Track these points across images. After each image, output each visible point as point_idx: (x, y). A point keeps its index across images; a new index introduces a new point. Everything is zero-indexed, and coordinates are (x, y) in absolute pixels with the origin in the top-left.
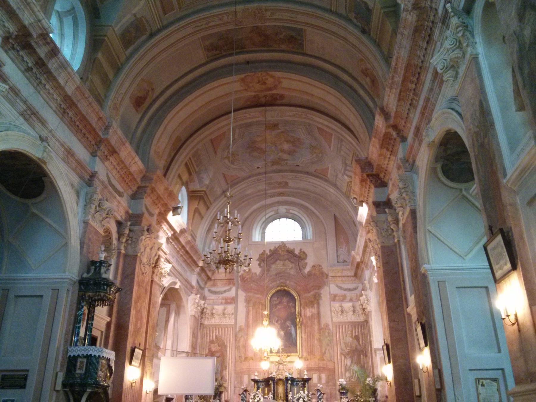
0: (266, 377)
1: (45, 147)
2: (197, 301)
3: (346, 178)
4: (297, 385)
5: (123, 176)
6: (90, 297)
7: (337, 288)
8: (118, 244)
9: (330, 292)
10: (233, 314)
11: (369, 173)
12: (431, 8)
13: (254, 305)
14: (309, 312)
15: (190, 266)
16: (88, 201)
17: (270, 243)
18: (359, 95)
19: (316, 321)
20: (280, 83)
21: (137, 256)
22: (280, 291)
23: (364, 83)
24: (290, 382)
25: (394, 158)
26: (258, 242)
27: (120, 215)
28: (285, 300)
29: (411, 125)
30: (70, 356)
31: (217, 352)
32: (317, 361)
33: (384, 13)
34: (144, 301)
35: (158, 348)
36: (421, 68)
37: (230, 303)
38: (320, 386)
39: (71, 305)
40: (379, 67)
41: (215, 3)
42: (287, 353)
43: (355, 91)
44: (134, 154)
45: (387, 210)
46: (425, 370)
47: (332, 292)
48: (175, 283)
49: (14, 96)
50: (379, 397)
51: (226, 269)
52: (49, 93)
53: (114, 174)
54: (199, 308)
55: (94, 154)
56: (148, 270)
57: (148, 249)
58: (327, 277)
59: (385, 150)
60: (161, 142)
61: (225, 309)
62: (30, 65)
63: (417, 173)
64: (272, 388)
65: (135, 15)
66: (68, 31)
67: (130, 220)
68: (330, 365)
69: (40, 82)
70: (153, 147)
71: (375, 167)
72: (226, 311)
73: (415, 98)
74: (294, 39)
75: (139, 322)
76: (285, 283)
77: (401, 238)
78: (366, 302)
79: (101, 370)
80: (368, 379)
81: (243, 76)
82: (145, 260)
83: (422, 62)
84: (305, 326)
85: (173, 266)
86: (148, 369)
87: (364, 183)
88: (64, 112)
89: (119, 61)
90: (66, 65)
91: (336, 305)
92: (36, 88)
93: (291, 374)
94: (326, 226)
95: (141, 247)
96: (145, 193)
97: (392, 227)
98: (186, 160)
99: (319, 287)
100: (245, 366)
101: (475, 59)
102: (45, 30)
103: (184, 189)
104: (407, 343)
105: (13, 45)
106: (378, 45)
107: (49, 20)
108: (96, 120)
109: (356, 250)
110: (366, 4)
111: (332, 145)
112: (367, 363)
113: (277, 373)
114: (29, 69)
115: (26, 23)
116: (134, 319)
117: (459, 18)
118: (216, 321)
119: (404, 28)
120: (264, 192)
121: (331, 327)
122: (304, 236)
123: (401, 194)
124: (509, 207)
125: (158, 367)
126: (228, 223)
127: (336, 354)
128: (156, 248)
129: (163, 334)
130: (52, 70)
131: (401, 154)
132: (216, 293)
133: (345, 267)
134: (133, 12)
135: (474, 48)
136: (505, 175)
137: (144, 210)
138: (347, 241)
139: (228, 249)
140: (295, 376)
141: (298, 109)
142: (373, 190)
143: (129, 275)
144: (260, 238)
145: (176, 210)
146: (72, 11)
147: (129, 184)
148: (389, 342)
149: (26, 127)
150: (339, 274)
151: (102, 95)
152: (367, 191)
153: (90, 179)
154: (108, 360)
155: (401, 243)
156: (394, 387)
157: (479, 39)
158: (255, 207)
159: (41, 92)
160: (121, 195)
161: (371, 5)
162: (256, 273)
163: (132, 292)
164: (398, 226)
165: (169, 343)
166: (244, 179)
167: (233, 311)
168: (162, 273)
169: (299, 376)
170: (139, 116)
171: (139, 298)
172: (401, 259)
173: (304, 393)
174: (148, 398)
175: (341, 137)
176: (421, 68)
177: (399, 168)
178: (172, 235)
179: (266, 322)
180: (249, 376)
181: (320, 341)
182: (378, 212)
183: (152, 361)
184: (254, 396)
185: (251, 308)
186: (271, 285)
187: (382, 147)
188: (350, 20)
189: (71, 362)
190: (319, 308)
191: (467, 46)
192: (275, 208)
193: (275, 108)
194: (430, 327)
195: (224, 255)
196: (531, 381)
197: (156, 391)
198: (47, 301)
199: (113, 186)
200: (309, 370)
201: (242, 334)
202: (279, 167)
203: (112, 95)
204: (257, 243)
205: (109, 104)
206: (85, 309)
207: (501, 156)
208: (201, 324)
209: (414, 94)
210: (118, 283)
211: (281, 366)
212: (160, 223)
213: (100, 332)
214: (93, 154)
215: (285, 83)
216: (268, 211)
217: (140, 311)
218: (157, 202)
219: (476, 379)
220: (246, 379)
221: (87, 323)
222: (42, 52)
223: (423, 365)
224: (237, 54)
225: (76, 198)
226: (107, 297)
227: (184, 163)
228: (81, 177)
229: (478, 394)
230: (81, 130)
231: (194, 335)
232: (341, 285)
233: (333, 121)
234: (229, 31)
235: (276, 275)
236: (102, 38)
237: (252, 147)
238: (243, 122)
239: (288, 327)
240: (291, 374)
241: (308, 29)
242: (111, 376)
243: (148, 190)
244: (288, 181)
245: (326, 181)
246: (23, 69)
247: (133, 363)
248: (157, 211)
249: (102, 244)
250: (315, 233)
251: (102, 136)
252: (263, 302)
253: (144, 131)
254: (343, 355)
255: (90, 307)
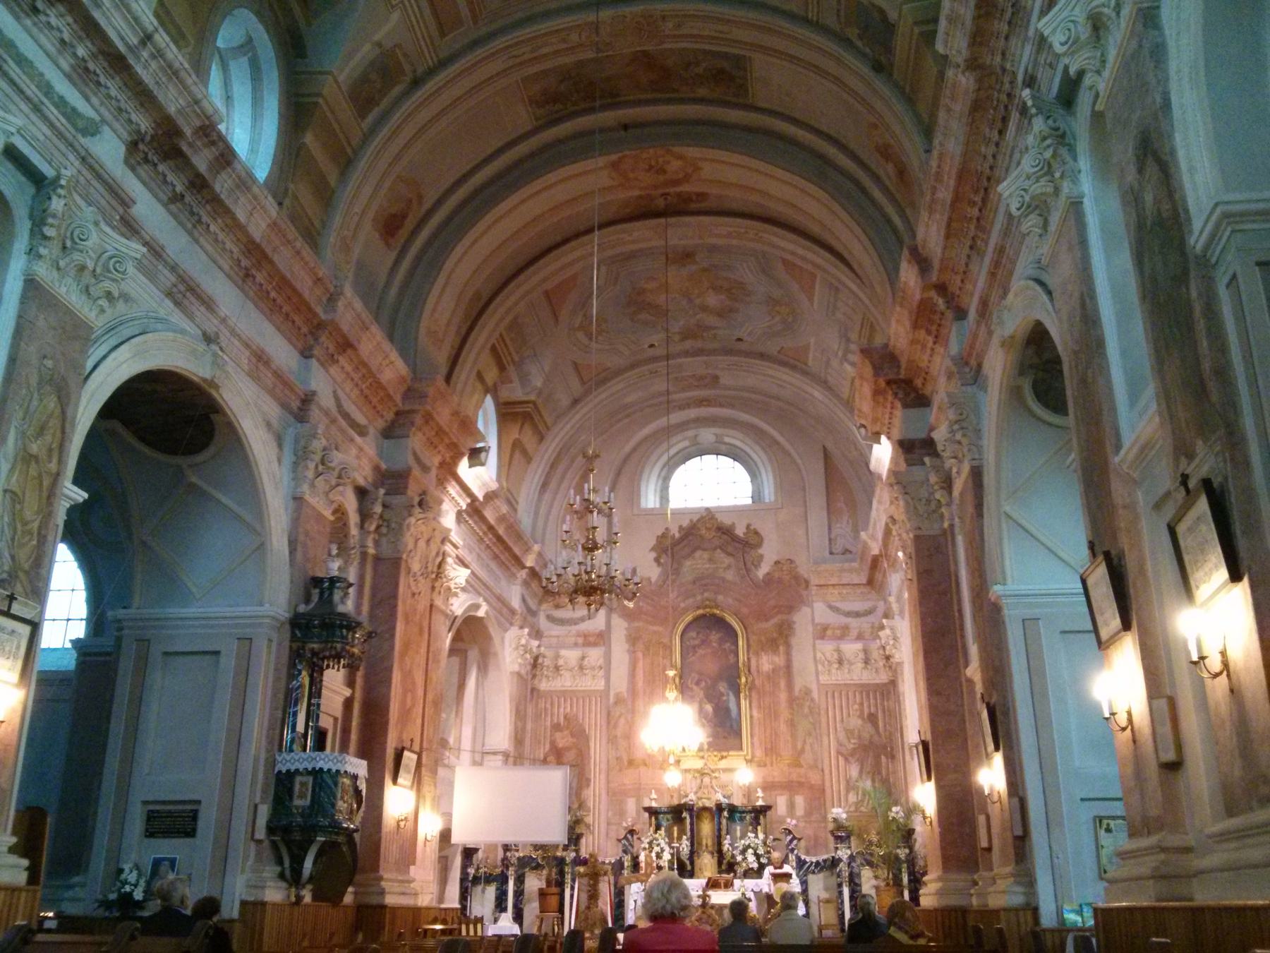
0: (675, 802)
1: (215, 355)
2: (523, 641)
3: (848, 368)
4: (742, 819)
5: (367, 392)
6: (314, 653)
7: (828, 610)
8: (361, 534)
9: (813, 620)
10: (601, 668)
11: (891, 376)
12: (1004, 70)
13: (647, 648)
14: (766, 662)
15: (508, 568)
16: (300, 453)
17: (677, 513)
18: (873, 201)
19: (783, 684)
20: (698, 169)
21: (400, 558)
22: (704, 616)
23: (881, 173)
24: (725, 813)
25: (942, 350)
26: (653, 509)
27: (363, 475)
28: (715, 636)
29: (975, 286)
30: (280, 772)
31: (568, 749)
32: (786, 768)
33: (921, 34)
34: (417, 652)
35: (444, 743)
36: (989, 179)
37: (595, 645)
38: (791, 823)
39: (276, 670)
40: (910, 145)
41: (554, 5)
42: (720, 751)
43: (864, 190)
44: (387, 346)
45: (927, 460)
46: (996, 798)
47: (817, 621)
48: (477, 607)
49: (154, 260)
50: (917, 847)
51: (589, 605)
52: (216, 240)
53: (348, 390)
54: (528, 656)
55: (307, 353)
56: (423, 585)
57: (422, 544)
58: (807, 586)
59: (923, 332)
60: (441, 308)
61: (583, 658)
62: (179, 188)
63: (984, 388)
64: (688, 827)
65: (379, 45)
66: (242, 90)
67: (382, 485)
68: (814, 778)
69: (199, 221)
70: (424, 324)
71: (903, 365)
72: (586, 662)
73: (980, 234)
74: (728, 77)
75: (409, 695)
76: (715, 601)
77: (957, 520)
78: (891, 642)
79: (342, 798)
80: (894, 809)
81: (614, 157)
82: (416, 567)
83: (991, 168)
84: (759, 693)
85: (473, 573)
86: (427, 788)
87: (881, 399)
88: (247, 275)
89: (349, 144)
90: (250, 182)
91: (827, 648)
92: (190, 234)
93: (728, 797)
94: (804, 472)
95: (409, 540)
96: (412, 424)
97: (938, 496)
98: (493, 340)
99: (791, 609)
100: (628, 778)
101: (1076, 206)
102: (208, 118)
103: (489, 402)
104: (966, 740)
105: (146, 154)
106: (910, 100)
107: (206, 86)
108: (310, 283)
109: (871, 530)
110: (882, 12)
111: (816, 298)
112: (894, 773)
113: (699, 794)
114: (177, 198)
115: (172, 110)
116: (400, 691)
117: (1048, 118)
118: (565, 682)
119: (953, 98)
120: (664, 399)
121: (815, 695)
122: (757, 496)
123: (952, 432)
124: (1121, 511)
125: (451, 784)
126: (591, 512)
127: (826, 754)
128: (438, 540)
129: (453, 715)
130: (223, 197)
131: (954, 349)
132: (562, 622)
133: (846, 565)
134: (377, 37)
135: (1075, 181)
136: (1118, 447)
137: (411, 461)
138: (852, 505)
139: (592, 566)
140: (738, 801)
141: (739, 220)
142: (899, 412)
143: (385, 600)
144: (658, 500)
145: (476, 456)
146: (247, 46)
147: (380, 408)
148: (929, 737)
149: (177, 318)
150: (834, 581)
151: (317, 223)
152: (887, 416)
153: (300, 407)
154: (355, 778)
155: (957, 530)
156: (937, 830)
157: (1084, 163)
158: (647, 431)
159: (201, 239)
160: (362, 432)
161: (893, 15)
162: (649, 579)
163: (393, 636)
164: (950, 493)
165: (467, 732)
166: (619, 372)
167: (601, 661)
168: (449, 589)
169: (745, 802)
170: (393, 255)
171: (407, 646)
172: (956, 564)
173: (757, 837)
174: (428, 849)
175: (836, 284)
176: (989, 179)
177: (950, 376)
178: (468, 505)
179: (672, 694)
180: (639, 800)
181: (792, 724)
182: (909, 463)
183: (434, 772)
184: (650, 843)
185: (640, 655)
186: (682, 605)
187: (915, 326)
188: (847, 43)
189: (283, 783)
190: (788, 654)
191: (1062, 177)
192: (691, 433)
193: (687, 219)
194: (1006, 713)
195: (585, 577)
196: (1149, 833)
197: (445, 836)
198: (228, 663)
199: (346, 416)
200: (768, 787)
201: (622, 713)
202: (699, 344)
203: (337, 220)
204: (650, 513)
205: (332, 239)
206: (305, 678)
207: (1113, 409)
208: (533, 690)
209: (977, 228)
210: (364, 617)
211: (707, 780)
212: (442, 484)
213: (331, 720)
214: (306, 354)
215: (707, 170)
216: (674, 440)
217: (410, 671)
218: (435, 440)
219: (1095, 817)
220: (631, 806)
221: (309, 705)
222: (201, 161)
223: (992, 789)
224: (604, 108)
225: (276, 450)
226: (348, 652)
227: (489, 346)
228: (284, 406)
229: (1098, 847)
230: (281, 308)
231: (519, 715)
232: (838, 605)
233: (817, 248)
234: (581, 64)
235: (694, 582)
236: (314, 99)
237: (638, 305)
238: (618, 250)
239: (722, 694)
240: (728, 797)
241: (758, 58)
242: (359, 808)
243: (418, 420)
244: (718, 373)
245: (805, 373)
246: (165, 198)
247: (400, 780)
248: (436, 460)
249: (331, 542)
250: (780, 487)
251: (323, 316)
252: (666, 640)
253: (405, 285)
254: (842, 755)
255: (313, 671)
